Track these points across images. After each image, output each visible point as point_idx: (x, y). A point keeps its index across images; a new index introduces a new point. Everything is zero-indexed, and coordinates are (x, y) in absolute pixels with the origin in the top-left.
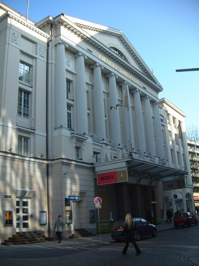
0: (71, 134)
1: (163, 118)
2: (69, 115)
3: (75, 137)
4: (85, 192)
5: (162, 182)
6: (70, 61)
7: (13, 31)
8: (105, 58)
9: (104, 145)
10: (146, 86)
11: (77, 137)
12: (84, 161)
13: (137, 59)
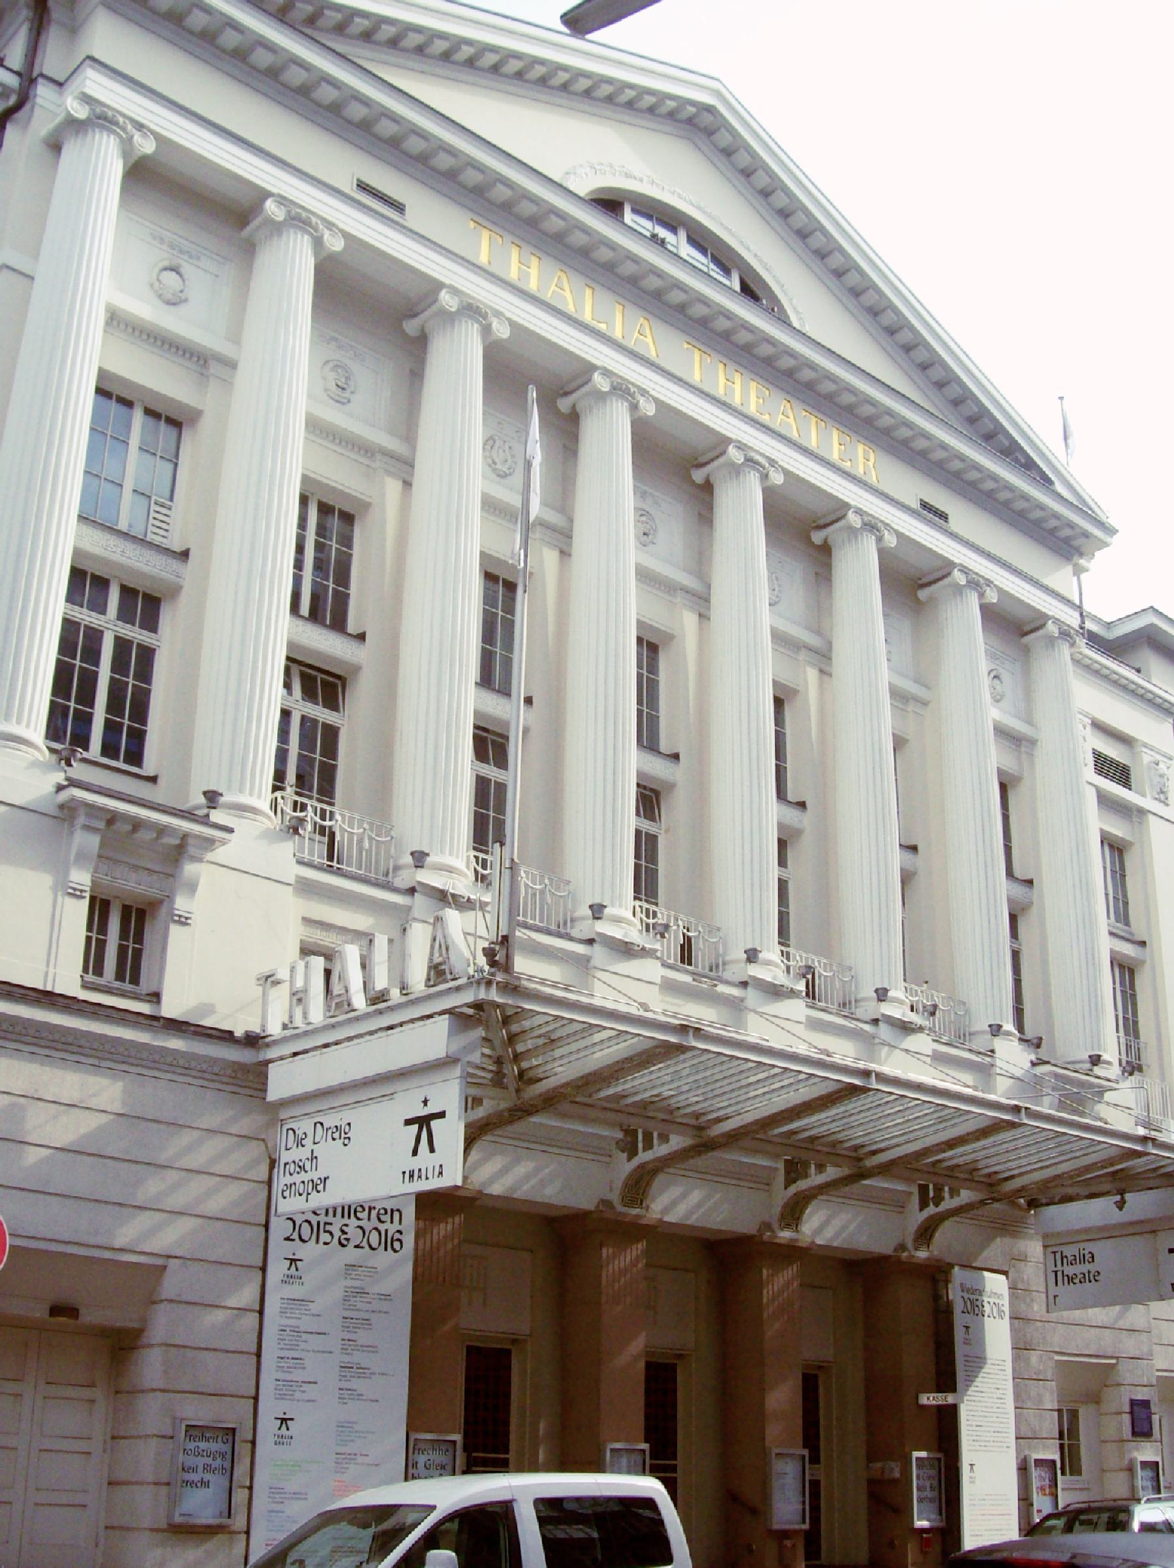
0: (1034, 1064)
1: (1135, 755)
2: (783, 885)
3: (91, 807)
4: (160, 1262)
5: (1045, 1236)
6: (187, 269)
7: (1151, 753)
8: (872, 456)
9: (884, 1031)
10: (941, 499)
11: (113, 818)
12: (170, 1008)
13: (852, 279)
